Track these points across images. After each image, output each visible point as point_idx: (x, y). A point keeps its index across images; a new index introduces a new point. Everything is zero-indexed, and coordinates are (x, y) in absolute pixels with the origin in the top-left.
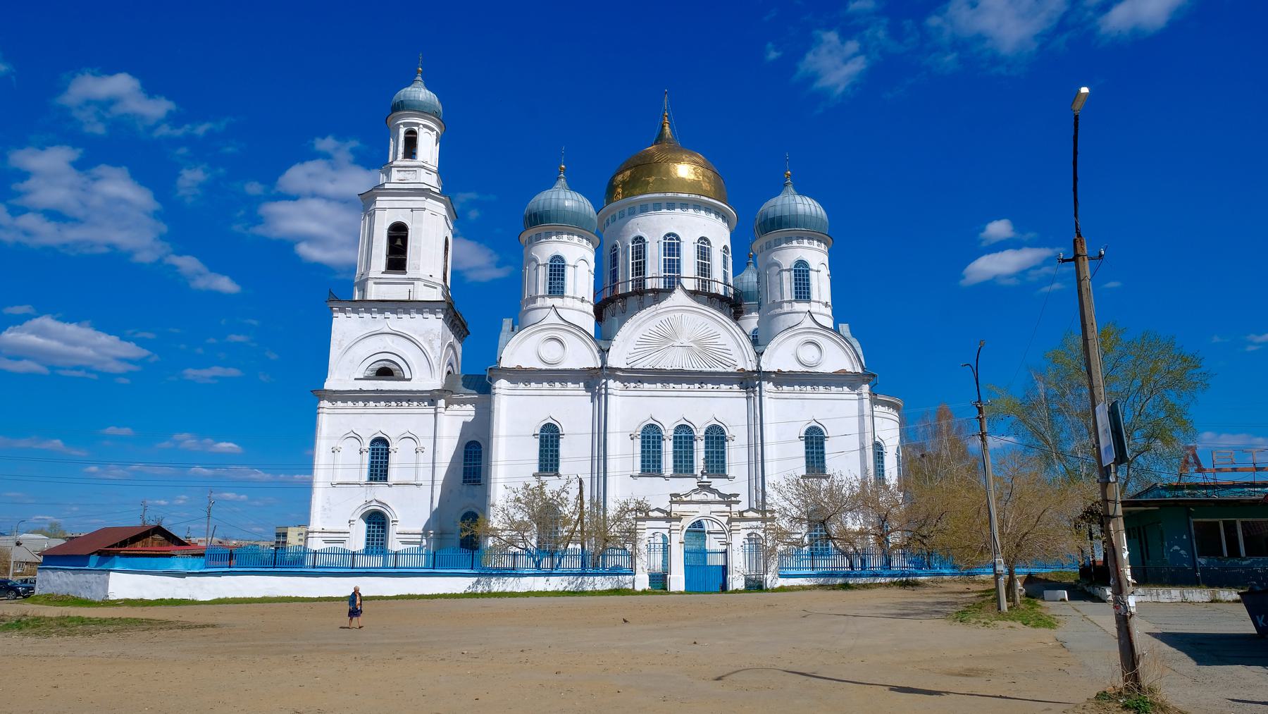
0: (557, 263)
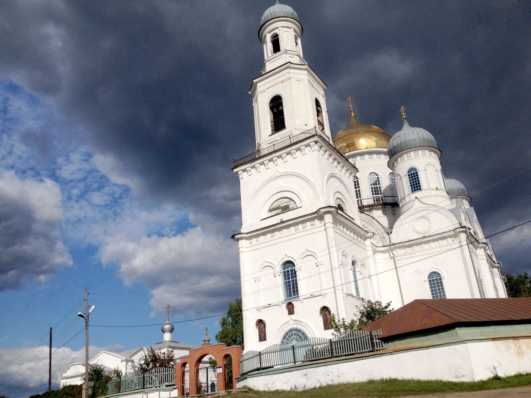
0: (412, 172)
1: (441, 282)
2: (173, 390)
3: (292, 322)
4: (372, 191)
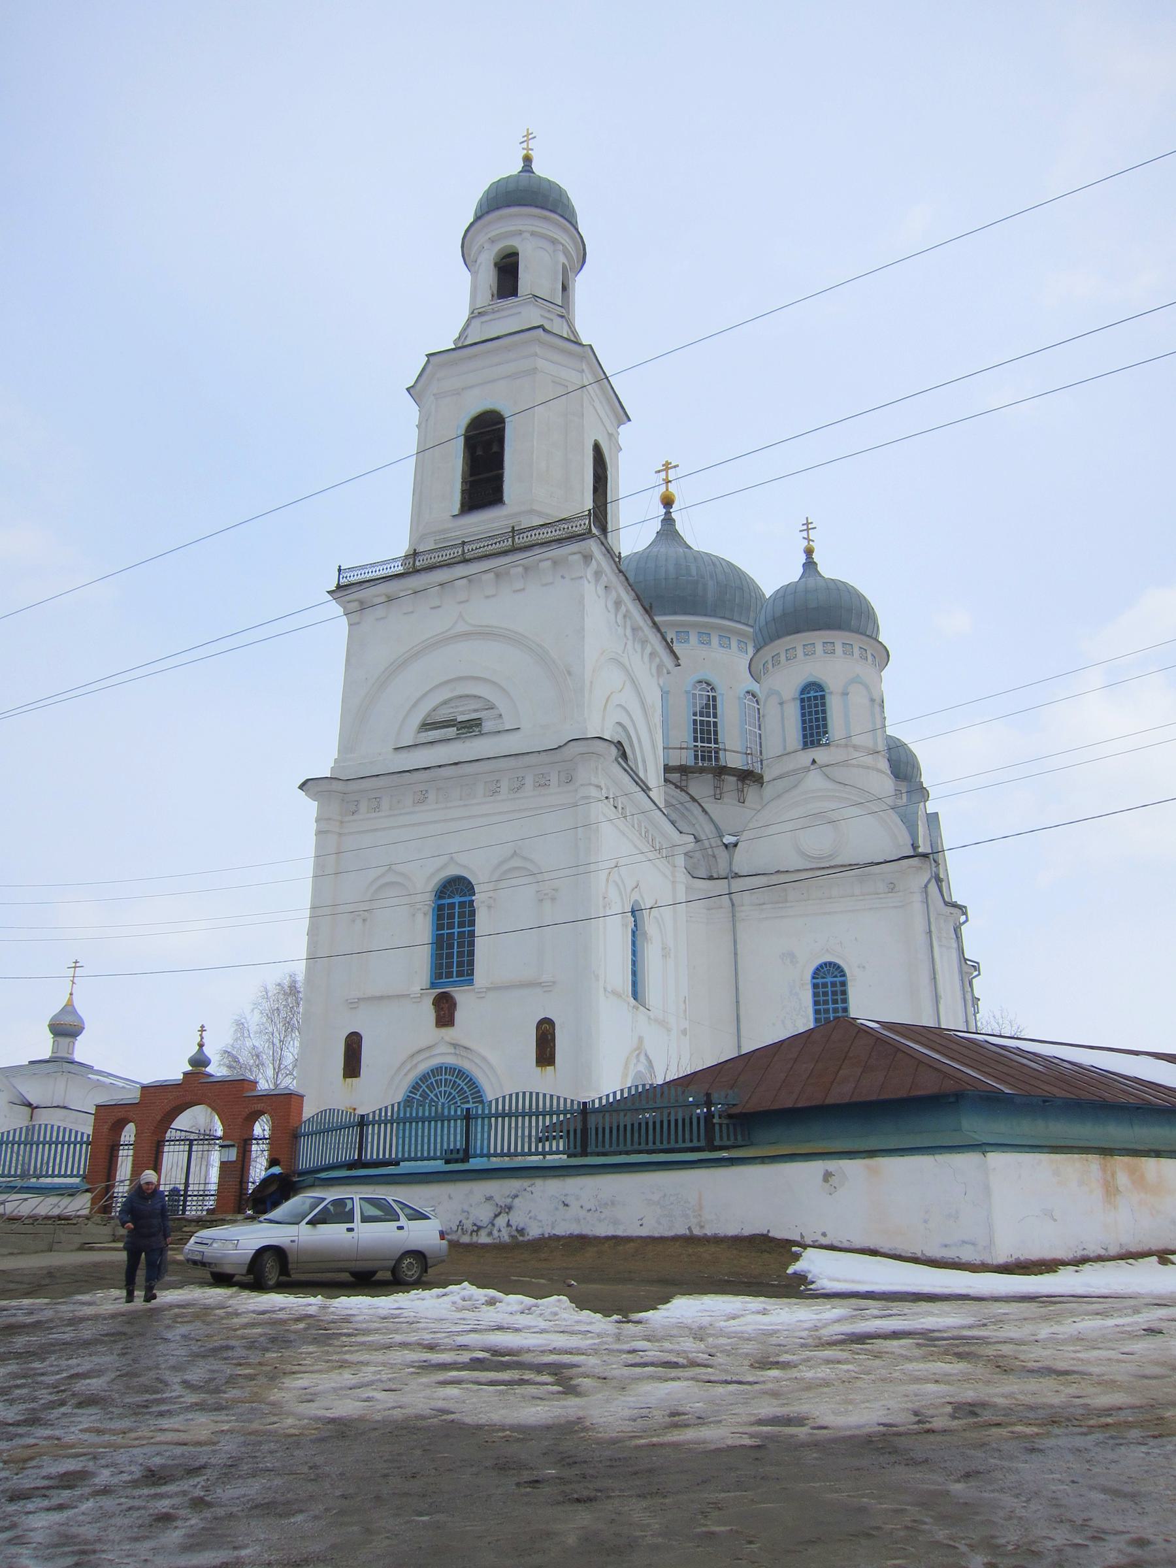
0: (812, 694)
1: (844, 993)
2: (588, 348)
3: (443, 1049)
4: (695, 731)
